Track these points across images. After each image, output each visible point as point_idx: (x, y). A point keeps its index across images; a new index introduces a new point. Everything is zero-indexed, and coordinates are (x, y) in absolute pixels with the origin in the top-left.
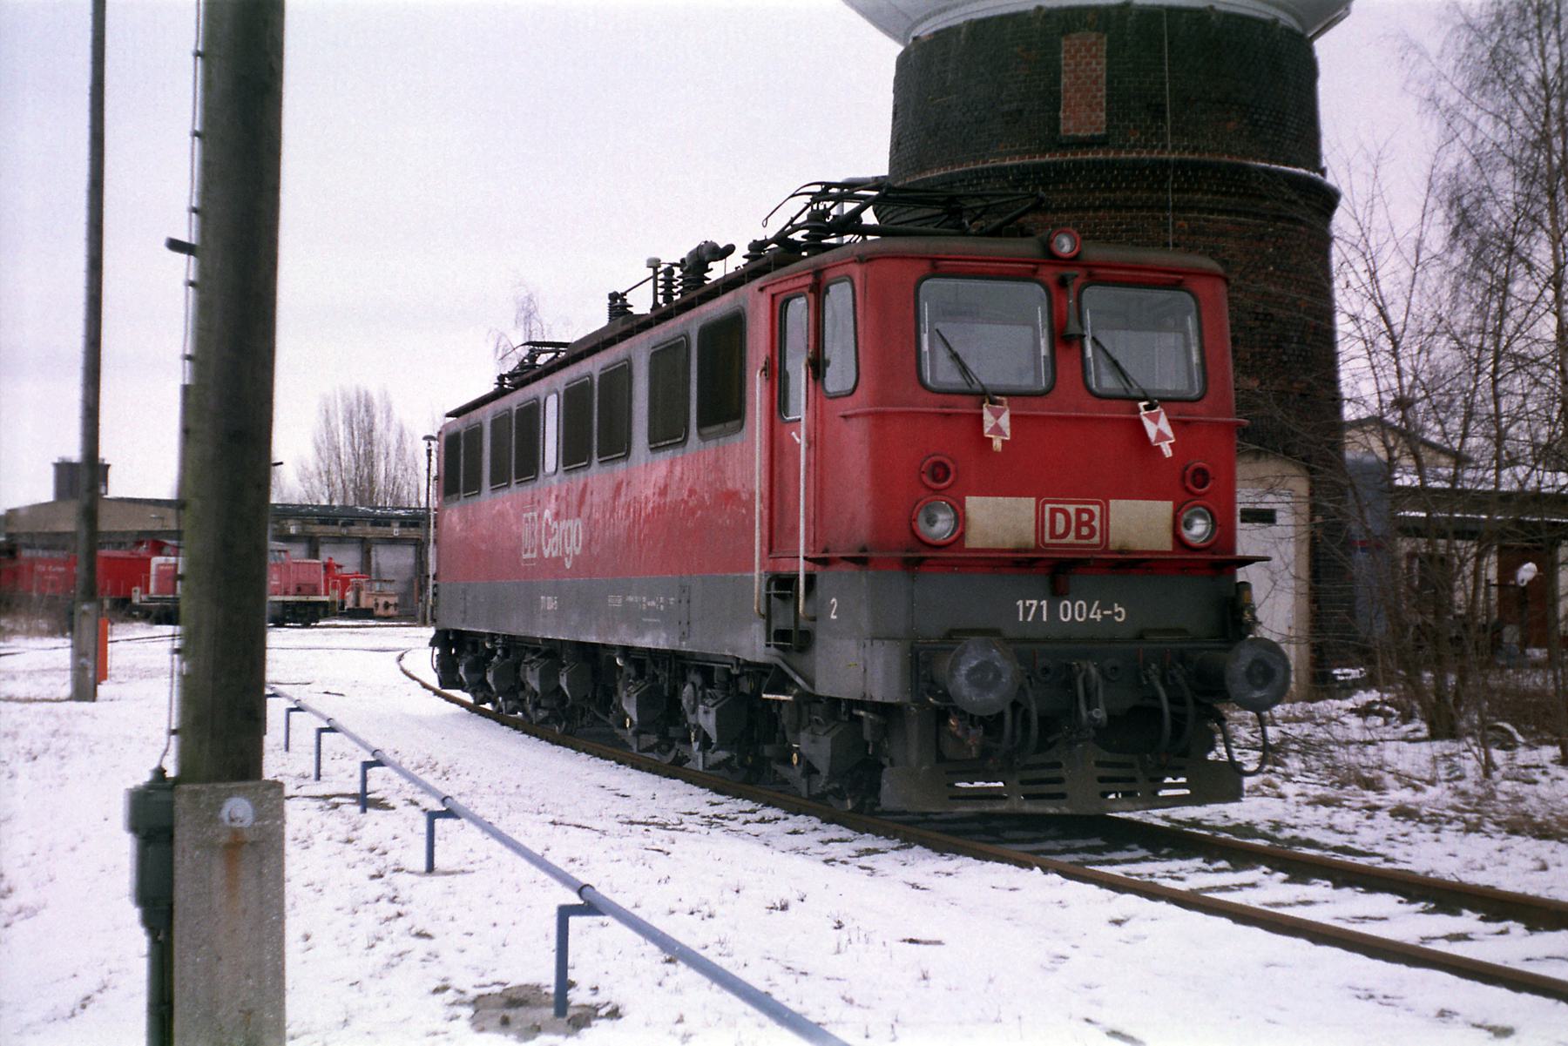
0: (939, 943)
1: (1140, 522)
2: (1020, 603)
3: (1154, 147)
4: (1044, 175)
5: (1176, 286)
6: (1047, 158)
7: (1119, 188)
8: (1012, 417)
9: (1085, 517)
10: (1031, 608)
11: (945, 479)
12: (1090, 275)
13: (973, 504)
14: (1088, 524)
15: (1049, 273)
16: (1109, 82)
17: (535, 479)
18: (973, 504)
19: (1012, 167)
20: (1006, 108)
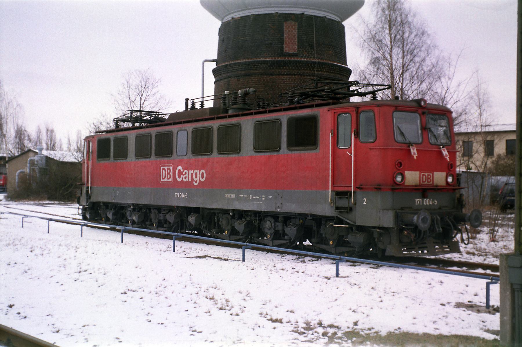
1: (440, 178)
3: (311, 57)
4: (279, 64)
6: (280, 59)
7: (302, 69)
8: (417, 150)
10: (418, 201)
11: (400, 167)
12: (396, 109)
13: (407, 173)
15: (420, 111)
16: (298, 37)
17: (171, 156)
18: (407, 173)
19: (270, 61)
20: (267, 42)
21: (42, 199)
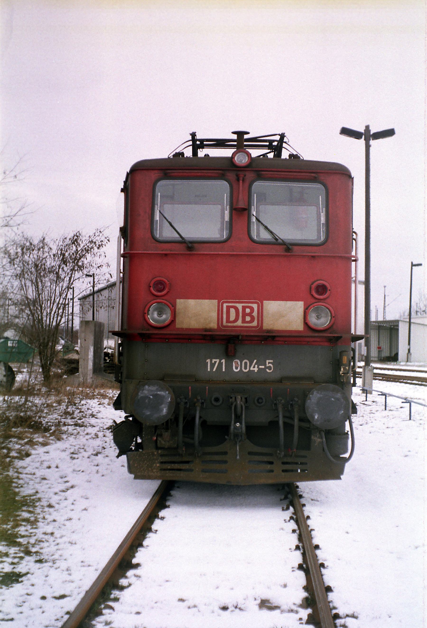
0: (420, 265)
2: (208, 361)
5: (314, 180)
9: (248, 311)
10: (215, 365)
14: (250, 314)
21: (386, 362)
